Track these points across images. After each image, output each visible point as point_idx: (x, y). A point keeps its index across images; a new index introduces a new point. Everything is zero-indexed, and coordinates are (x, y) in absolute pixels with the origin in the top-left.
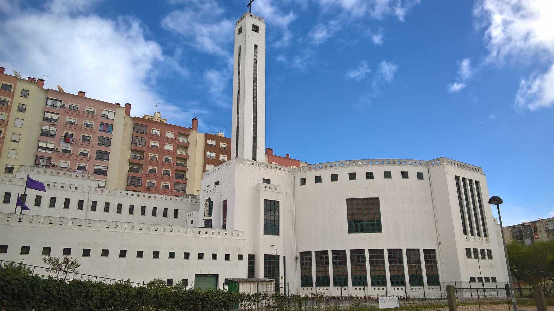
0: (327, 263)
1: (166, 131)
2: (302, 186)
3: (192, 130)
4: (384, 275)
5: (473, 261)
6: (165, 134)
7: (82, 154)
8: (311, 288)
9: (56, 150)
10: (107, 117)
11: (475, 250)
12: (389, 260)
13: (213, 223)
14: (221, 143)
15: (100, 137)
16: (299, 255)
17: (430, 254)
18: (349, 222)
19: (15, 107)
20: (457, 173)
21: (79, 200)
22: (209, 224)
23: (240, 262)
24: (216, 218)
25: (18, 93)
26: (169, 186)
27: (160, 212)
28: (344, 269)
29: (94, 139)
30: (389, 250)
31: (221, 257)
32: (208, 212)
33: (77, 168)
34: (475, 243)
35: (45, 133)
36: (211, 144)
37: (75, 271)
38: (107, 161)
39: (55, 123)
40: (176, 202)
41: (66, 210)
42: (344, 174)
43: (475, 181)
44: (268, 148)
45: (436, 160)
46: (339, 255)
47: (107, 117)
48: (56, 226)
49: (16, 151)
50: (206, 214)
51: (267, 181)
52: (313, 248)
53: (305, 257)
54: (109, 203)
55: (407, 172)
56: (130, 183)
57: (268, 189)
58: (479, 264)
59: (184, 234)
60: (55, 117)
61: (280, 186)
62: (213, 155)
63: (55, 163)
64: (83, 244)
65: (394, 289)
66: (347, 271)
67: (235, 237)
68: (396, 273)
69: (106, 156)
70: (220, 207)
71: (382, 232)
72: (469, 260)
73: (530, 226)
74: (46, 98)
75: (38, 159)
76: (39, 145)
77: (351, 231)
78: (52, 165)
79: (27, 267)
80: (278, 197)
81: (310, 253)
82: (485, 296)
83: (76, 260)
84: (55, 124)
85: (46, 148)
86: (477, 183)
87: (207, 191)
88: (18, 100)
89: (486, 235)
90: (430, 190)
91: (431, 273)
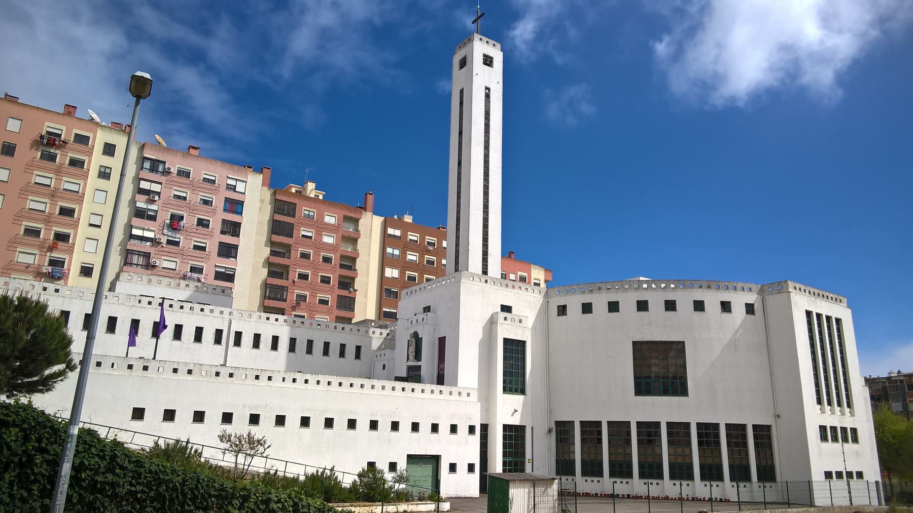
1: (325, 213)
2: (560, 317)
3: (364, 212)
4: (689, 463)
5: (830, 445)
6: (323, 217)
7: (196, 248)
8: (573, 477)
9: (157, 241)
10: (235, 189)
11: (834, 429)
12: (698, 440)
13: (423, 372)
14: (409, 233)
15: (224, 221)
16: (553, 426)
17: (763, 433)
18: (636, 378)
19: (93, 172)
20: (809, 306)
21: (216, 329)
22: (416, 373)
23: (471, 437)
24: (427, 364)
25: (98, 148)
26: (328, 301)
27: (334, 349)
28: (628, 451)
29: (215, 225)
31: (444, 429)
32: (414, 354)
33: (189, 271)
34: (834, 418)
35: (140, 214)
36: (394, 235)
37: (264, 455)
38: (235, 259)
39: (157, 198)
40: (358, 334)
41: (198, 344)
42: (628, 301)
43: (826, 316)
45: (776, 284)
46: (619, 429)
47: (233, 188)
48: (210, 378)
49: (96, 241)
50: (411, 357)
51: (506, 309)
52: (577, 415)
53: (563, 430)
54: (259, 335)
55: (730, 302)
56: (269, 294)
57: (508, 322)
58: (844, 453)
59: (390, 392)
60: (156, 188)
61: (527, 317)
62: (397, 252)
63: (156, 262)
64: (249, 407)
66: (631, 454)
67: (464, 397)
68: (709, 461)
69: (233, 251)
70: (433, 346)
71: (688, 396)
72: (824, 444)
73: (901, 381)
74: (142, 157)
75: (130, 256)
76: (132, 233)
77: (639, 392)
78: (152, 264)
79: (195, 447)
80: (524, 334)
82: (851, 504)
83: (265, 438)
84: (156, 199)
85: (142, 239)
86: (838, 321)
87: (412, 321)
88: (97, 160)
89: (849, 405)
90: (764, 331)
91: (763, 463)
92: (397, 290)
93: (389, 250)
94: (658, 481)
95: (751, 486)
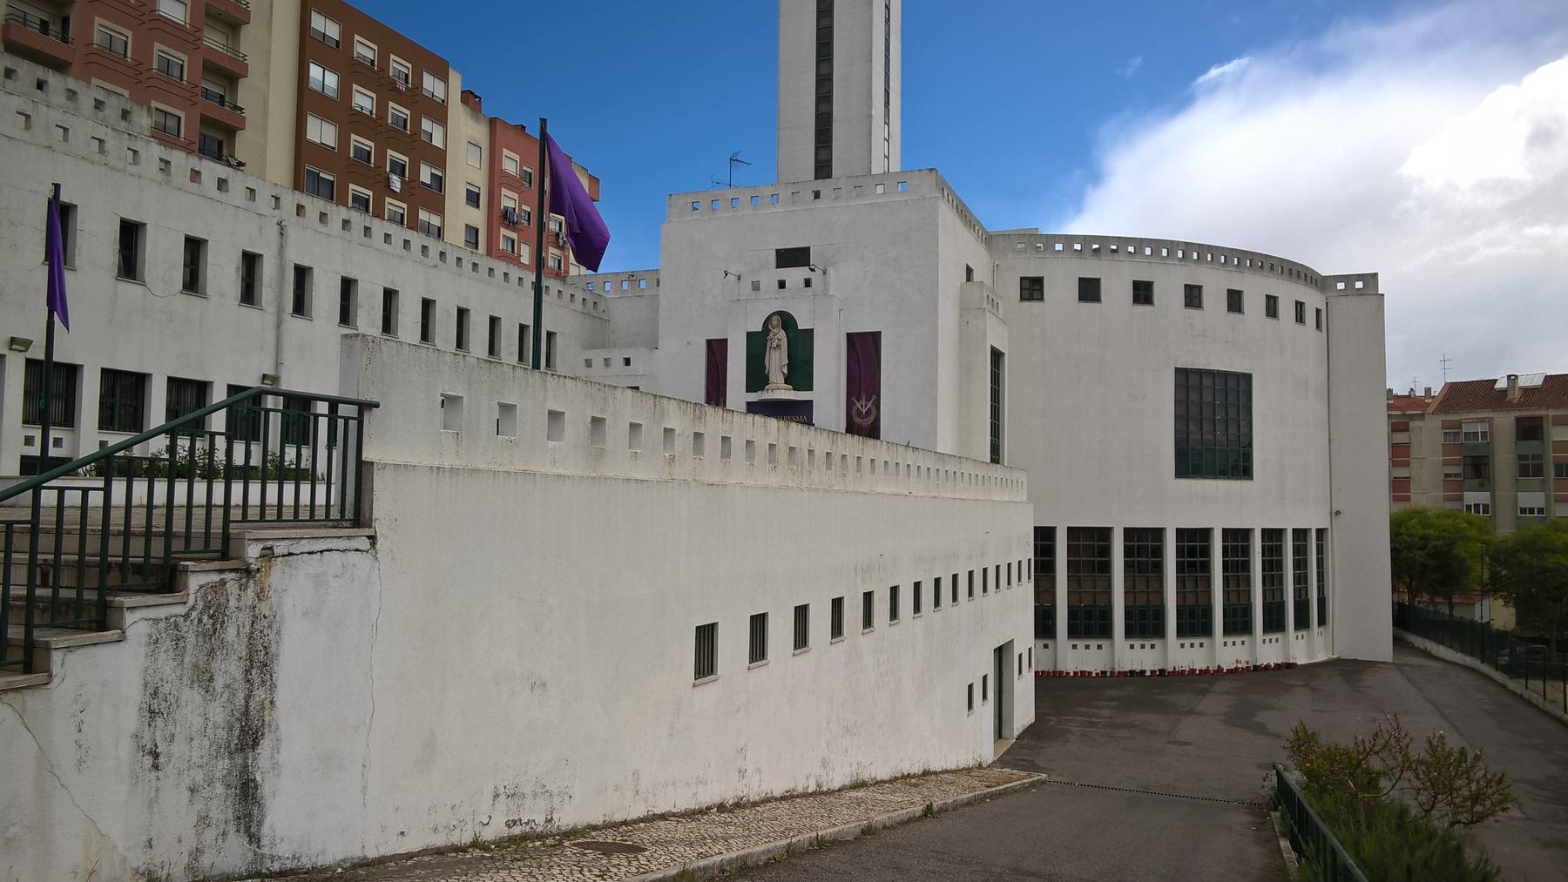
0: (1106, 567)
30: (1128, 532)
43: (478, 207)
44: (471, 93)
46: (1144, 543)
62: (332, 80)
65: (1132, 647)
71: (1252, 479)
81: (1158, 533)
92: (332, 179)
93: (315, 72)
94: (1202, 640)
95: (1213, 646)
